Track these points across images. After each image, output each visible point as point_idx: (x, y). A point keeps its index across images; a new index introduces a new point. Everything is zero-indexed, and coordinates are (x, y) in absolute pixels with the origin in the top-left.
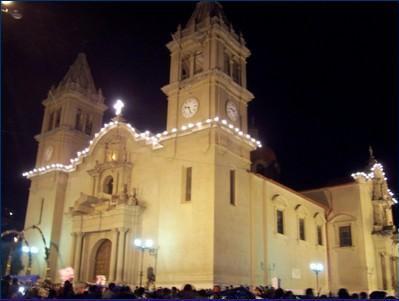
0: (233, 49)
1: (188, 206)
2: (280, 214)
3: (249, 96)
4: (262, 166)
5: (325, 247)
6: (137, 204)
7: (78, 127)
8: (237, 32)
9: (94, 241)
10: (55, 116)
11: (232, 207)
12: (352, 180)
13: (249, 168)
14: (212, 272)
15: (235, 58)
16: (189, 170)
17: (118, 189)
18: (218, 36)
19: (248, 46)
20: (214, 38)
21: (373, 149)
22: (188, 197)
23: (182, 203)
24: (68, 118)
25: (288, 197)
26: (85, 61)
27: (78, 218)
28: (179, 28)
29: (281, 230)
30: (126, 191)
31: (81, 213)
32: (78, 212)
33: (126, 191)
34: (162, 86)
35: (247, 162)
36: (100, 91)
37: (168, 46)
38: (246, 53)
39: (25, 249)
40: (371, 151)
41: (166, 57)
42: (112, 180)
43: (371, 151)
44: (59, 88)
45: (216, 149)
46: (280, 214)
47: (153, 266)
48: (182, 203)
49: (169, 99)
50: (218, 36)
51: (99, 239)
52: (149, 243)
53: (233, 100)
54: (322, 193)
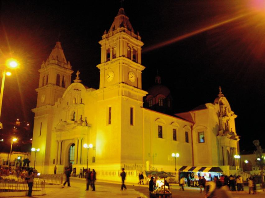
0: (133, 43)
1: (110, 127)
2: (160, 128)
3: (142, 68)
4: (147, 104)
5: (190, 144)
6: (87, 125)
7: (58, 84)
8: (136, 33)
9: (66, 145)
10: (45, 78)
11: (132, 126)
12: (206, 108)
13: (142, 106)
14: (120, 159)
15: (134, 48)
16: (110, 109)
17: (77, 118)
18: (124, 38)
19: (142, 40)
20: (122, 39)
21: (221, 88)
22: (110, 123)
23: (107, 125)
24: (52, 80)
25: (165, 120)
26: (60, 46)
27: (59, 133)
28: (105, 32)
29: (160, 135)
30: (81, 118)
31: (61, 130)
32: (58, 129)
33: (81, 118)
34: (97, 65)
35: (141, 103)
36: (69, 63)
37: (100, 42)
38: (141, 44)
39: (85, 146)
40: (220, 89)
41: (98, 48)
42: (75, 113)
43: (220, 89)
44: (46, 63)
45: (122, 98)
46: (160, 128)
47: (95, 156)
48: (107, 125)
49: (100, 71)
50: (124, 38)
51: (69, 143)
52: (91, 146)
53: (133, 71)
54: (190, 114)
